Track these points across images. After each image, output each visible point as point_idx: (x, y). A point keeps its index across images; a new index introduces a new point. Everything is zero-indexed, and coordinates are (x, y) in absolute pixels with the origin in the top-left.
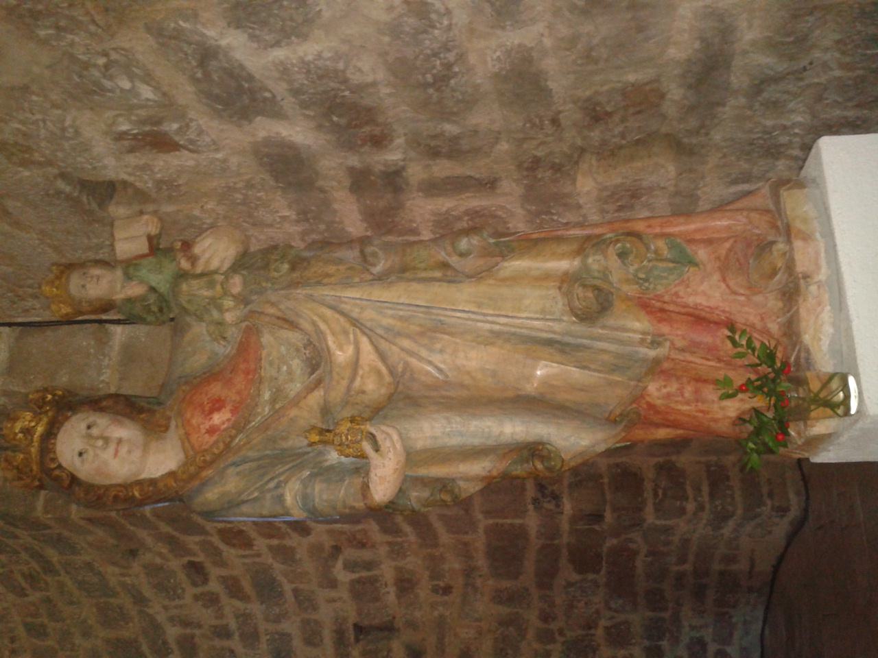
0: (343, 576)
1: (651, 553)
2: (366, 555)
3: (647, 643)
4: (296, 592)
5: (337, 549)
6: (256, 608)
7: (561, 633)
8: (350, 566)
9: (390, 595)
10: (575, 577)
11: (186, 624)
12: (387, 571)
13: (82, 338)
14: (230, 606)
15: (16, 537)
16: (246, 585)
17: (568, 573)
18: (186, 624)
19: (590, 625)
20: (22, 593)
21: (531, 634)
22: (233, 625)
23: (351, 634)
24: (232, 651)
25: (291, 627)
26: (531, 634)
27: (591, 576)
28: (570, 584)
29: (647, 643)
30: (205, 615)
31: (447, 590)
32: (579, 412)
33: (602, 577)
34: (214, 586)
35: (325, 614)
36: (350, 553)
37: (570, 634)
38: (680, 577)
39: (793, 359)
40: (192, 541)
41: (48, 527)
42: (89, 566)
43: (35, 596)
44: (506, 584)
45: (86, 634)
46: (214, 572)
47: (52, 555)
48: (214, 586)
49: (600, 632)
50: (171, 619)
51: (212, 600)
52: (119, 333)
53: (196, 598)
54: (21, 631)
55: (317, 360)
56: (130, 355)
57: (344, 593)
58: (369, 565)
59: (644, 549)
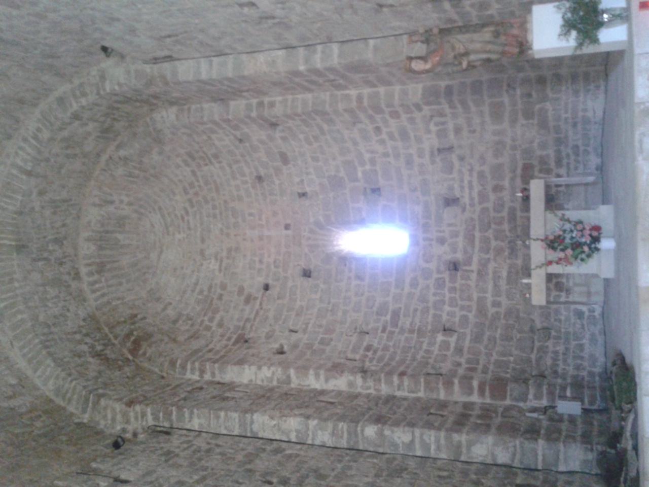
0: (433, 128)
1: (553, 110)
2: (442, 119)
3: (555, 148)
4: (415, 136)
5: (432, 116)
6: (399, 144)
7: (520, 146)
8: (436, 124)
9: (452, 136)
10: (524, 122)
11: (372, 152)
12: (451, 126)
13: (361, 45)
14: (390, 143)
15: (315, 119)
16: (396, 135)
17: (521, 120)
18: (372, 152)
19: (532, 142)
20: (310, 144)
21: (508, 148)
22: (390, 151)
23: (436, 153)
24: (389, 162)
25: (413, 151)
26: (508, 148)
27: (531, 121)
28: (523, 125)
29: (555, 148)
30: (380, 149)
31: (474, 131)
32: (603, 195)
33: (535, 121)
34: (384, 136)
35: (426, 146)
36: (437, 119)
37: (523, 147)
38: (566, 119)
39: (13, 243)
40: (378, 117)
41: (328, 114)
42: (338, 131)
43: (316, 145)
44: (497, 127)
45: (334, 159)
46: (384, 130)
47: (325, 127)
48: (384, 136)
49: (535, 145)
50: (367, 151)
51: (382, 142)
52: (371, 42)
53: (377, 141)
54: (309, 160)
55: (453, 48)
56: (376, 49)
57: (434, 136)
58: (443, 123)
59: (551, 109)
